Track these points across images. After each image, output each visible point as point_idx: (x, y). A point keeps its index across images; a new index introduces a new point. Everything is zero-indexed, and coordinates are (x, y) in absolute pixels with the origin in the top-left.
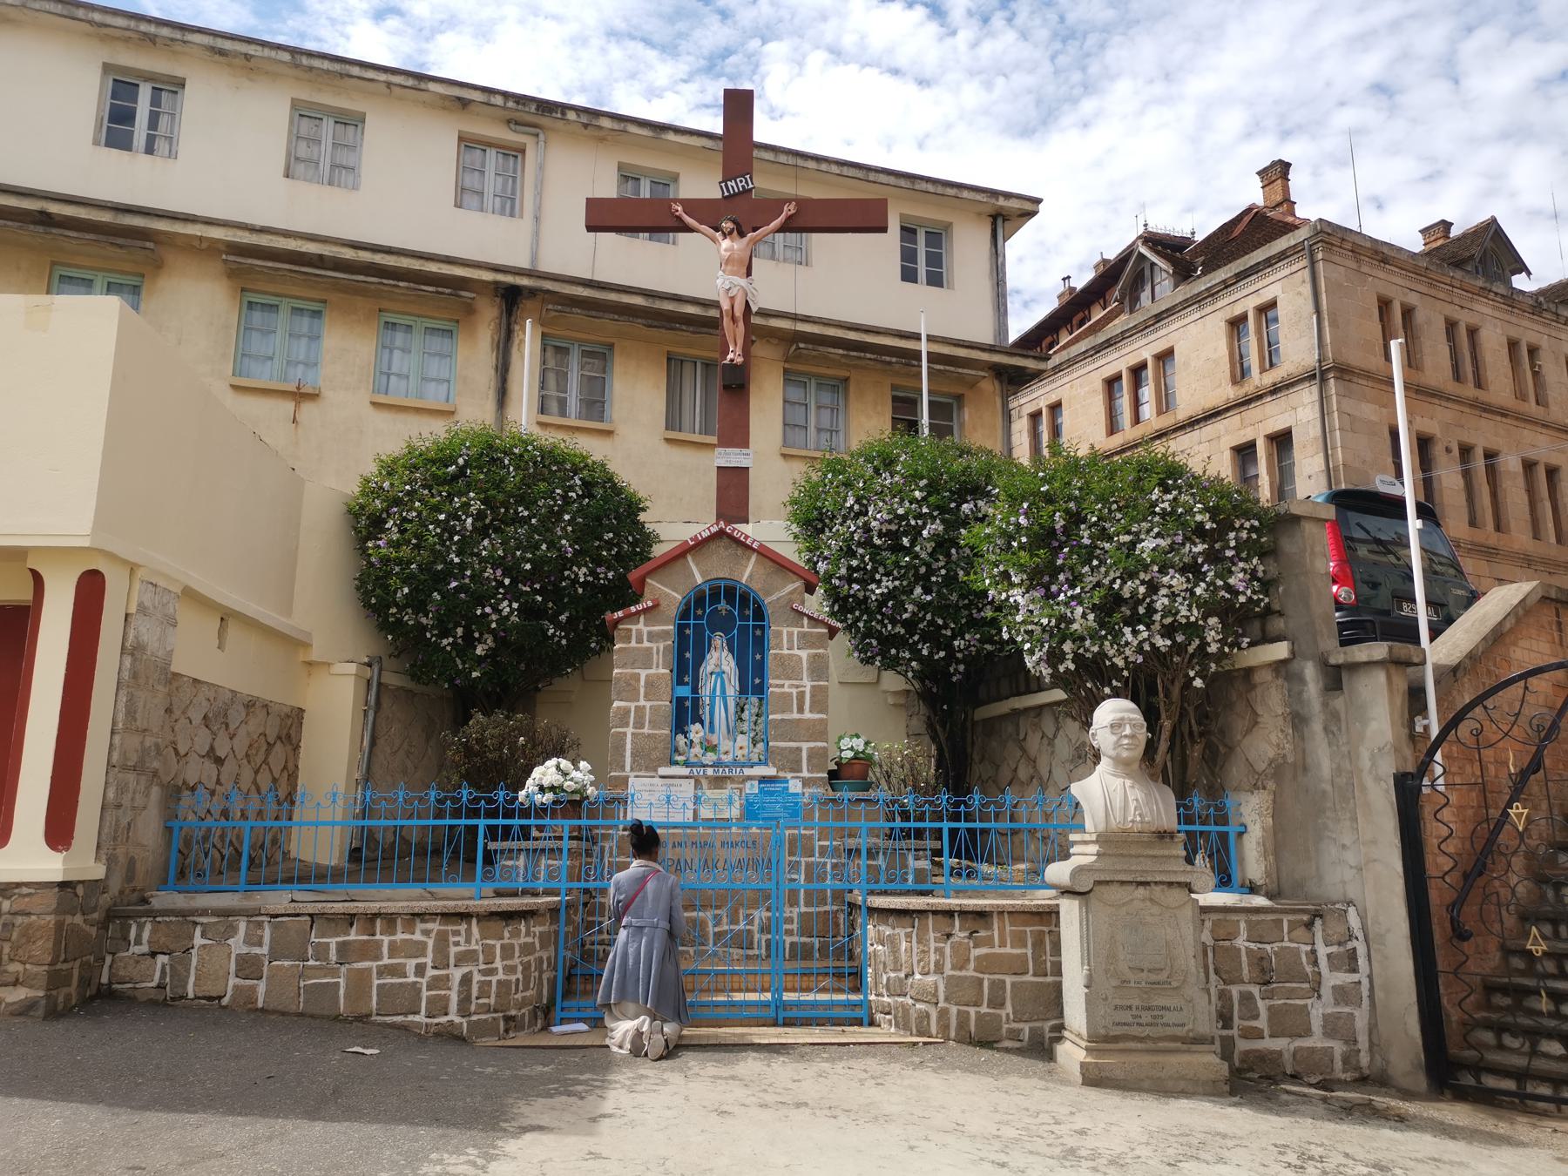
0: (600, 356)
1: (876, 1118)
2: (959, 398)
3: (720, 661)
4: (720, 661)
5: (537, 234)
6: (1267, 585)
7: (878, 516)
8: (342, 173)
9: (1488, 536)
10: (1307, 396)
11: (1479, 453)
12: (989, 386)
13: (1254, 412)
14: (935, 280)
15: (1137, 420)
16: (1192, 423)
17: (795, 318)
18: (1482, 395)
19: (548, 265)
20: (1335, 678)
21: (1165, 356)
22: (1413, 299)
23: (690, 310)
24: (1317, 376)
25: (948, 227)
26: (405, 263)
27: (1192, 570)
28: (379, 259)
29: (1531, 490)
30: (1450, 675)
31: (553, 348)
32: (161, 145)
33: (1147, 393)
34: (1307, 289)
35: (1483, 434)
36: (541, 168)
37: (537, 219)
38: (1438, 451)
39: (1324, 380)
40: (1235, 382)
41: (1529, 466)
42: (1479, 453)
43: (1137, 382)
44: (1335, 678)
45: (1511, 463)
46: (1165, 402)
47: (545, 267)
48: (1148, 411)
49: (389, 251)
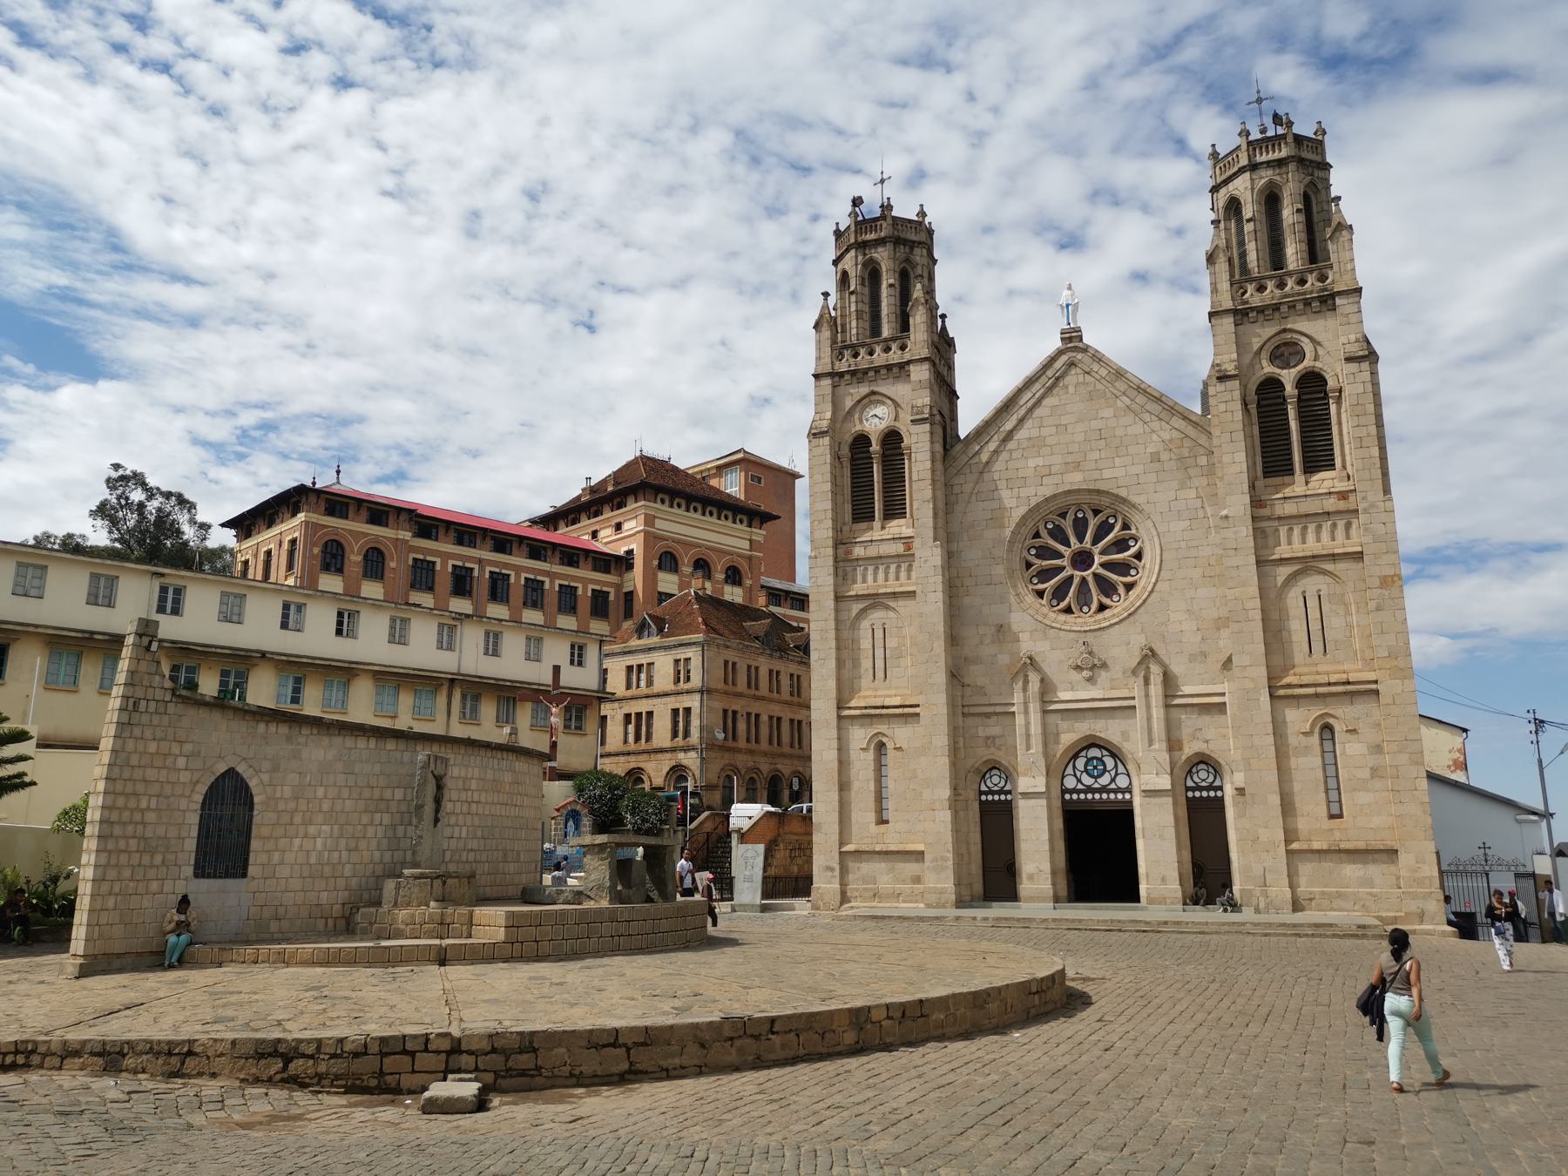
0: (477, 698)
1: (1090, 653)
2: (586, 706)
3: (571, 823)
4: (571, 823)
5: (460, 658)
6: (667, 816)
7: (598, 792)
8: (403, 641)
9: (753, 745)
10: (697, 697)
11: (753, 715)
12: (595, 702)
13: (680, 698)
14: (580, 664)
15: (638, 686)
16: (658, 696)
17: (539, 684)
18: (757, 693)
19: (463, 671)
20: (675, 832)
21: (650, 664)
22: (736, 660)
23: (508, 684)
24: (701, 692)
25: (585, 644)
26: (427, 674)
27: (656, 814)
28: (420, 673)
29: (771, 727)
30: (691, 831)
31: (464, 697)
32: (351, 634)
33: (643, 676)
34: (701, 658)
35: (755, 707)
36: (461, 634)
37: (461, 652)
38: (739, 716)
39: (702, 694)
40: (675, 684)
41: (771, 718)
42: (753, 715)
43: (639, 671)
44: (675, 832)
45: (764, 718)
46: (650, 683)
47: (462, 672)
48: (643, 683)
49: (423, 670)
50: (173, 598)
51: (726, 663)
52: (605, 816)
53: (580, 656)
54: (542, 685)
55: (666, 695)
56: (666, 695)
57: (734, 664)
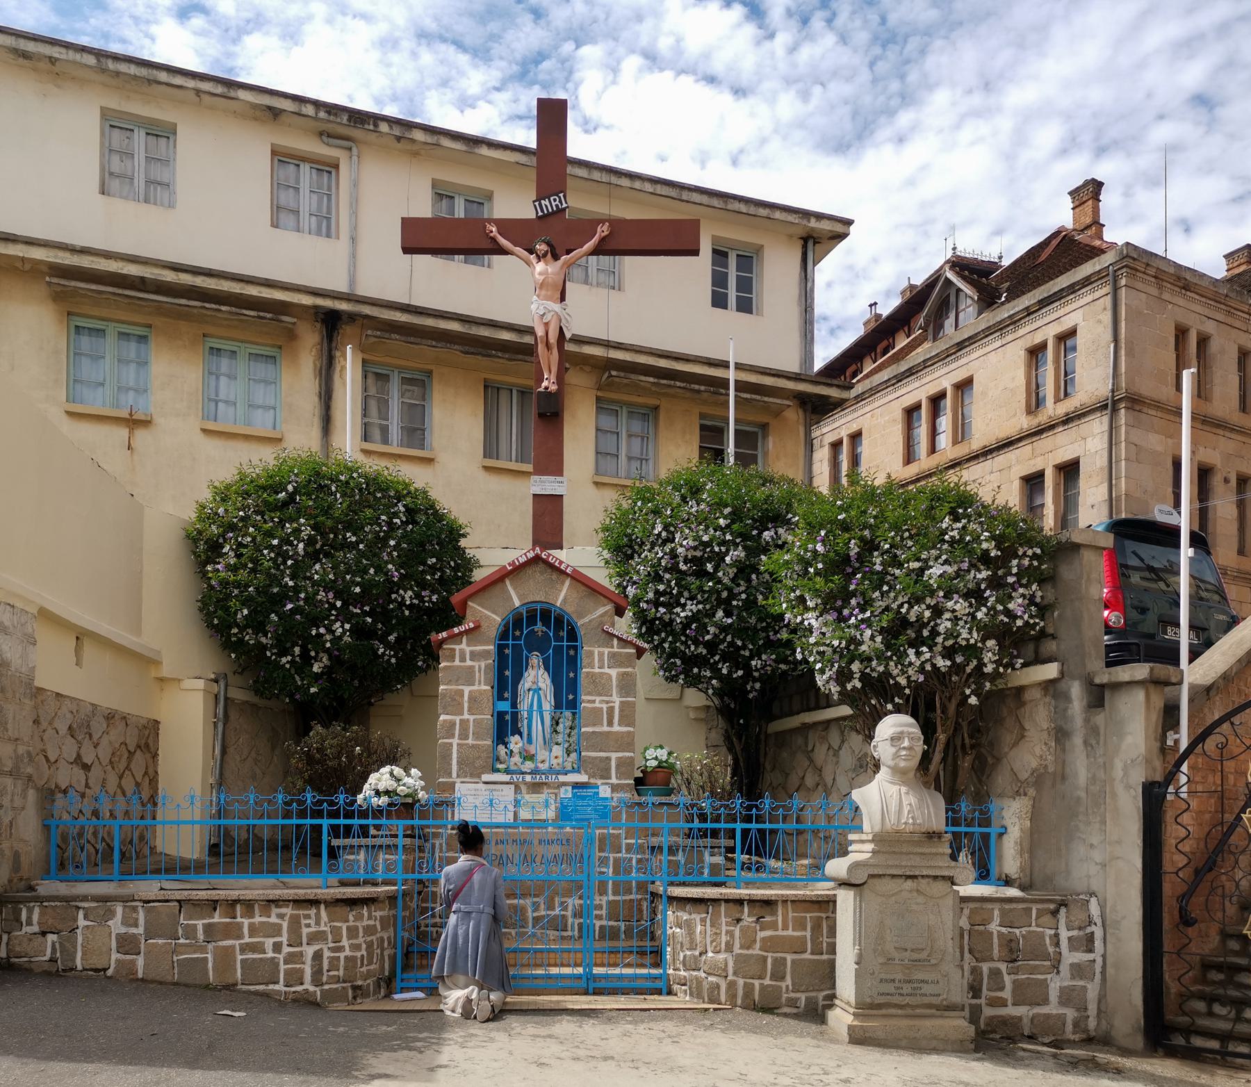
0: (419, 382)
2: (764, 427)
6: (1043, 610)
7: (684, 543)
10: (1098, 426)
12: (794, 415)
13: (1046, 442)
14: (745, 306)
15: (933, 449)
16: (986, 453)
17: (608, 344)
20: (1098, 696)
21: (964, 386)
22: (1210, 327)
23: (506, 336)
24: (1109, 406)
25: (759, 249)
26: (236, 288)
27: (975, 595)
30: (1203, 694)
31: (374, 375)
33: (945, 422)
34: (1107, 317)
36: (355, 184)
37: (353, 240)
38: (1216, 481)
39: (1115, 410)
43: (935, 410)
46: (961, 431)
48: (944, 440)
49: (209, 273)
50: (980, 826)
51: (1181, 333)
52: (732, 656)
53: (745, 285)
54: (619, 346)
55: (1007, 444)
56: (1007, 444)
57: (1203, 341)
